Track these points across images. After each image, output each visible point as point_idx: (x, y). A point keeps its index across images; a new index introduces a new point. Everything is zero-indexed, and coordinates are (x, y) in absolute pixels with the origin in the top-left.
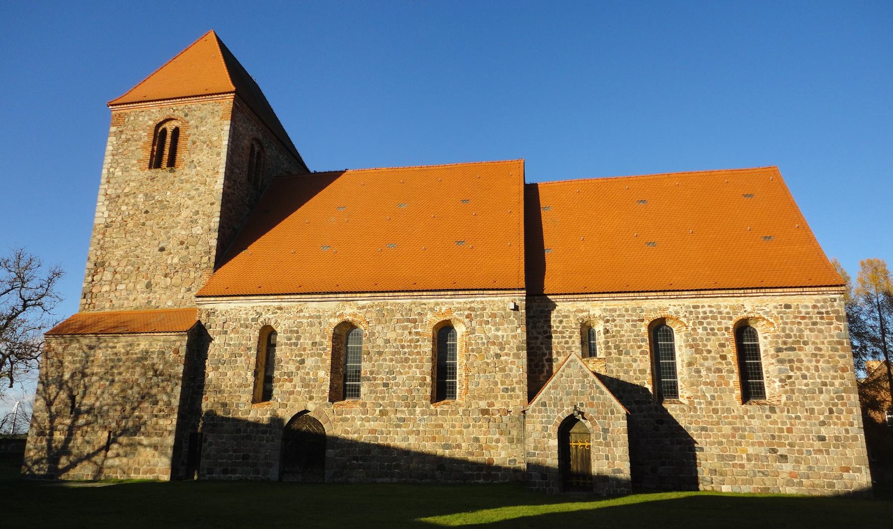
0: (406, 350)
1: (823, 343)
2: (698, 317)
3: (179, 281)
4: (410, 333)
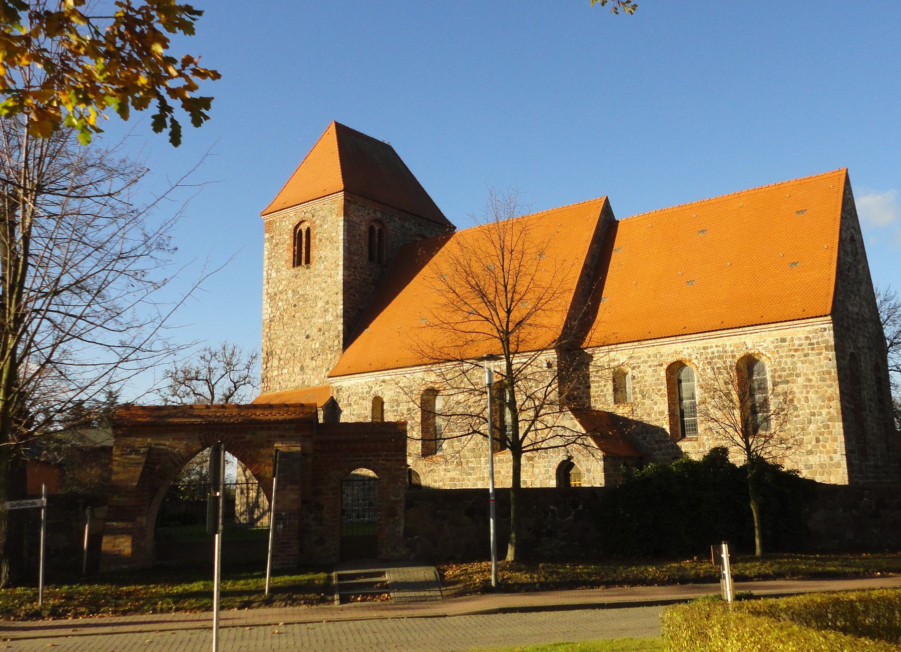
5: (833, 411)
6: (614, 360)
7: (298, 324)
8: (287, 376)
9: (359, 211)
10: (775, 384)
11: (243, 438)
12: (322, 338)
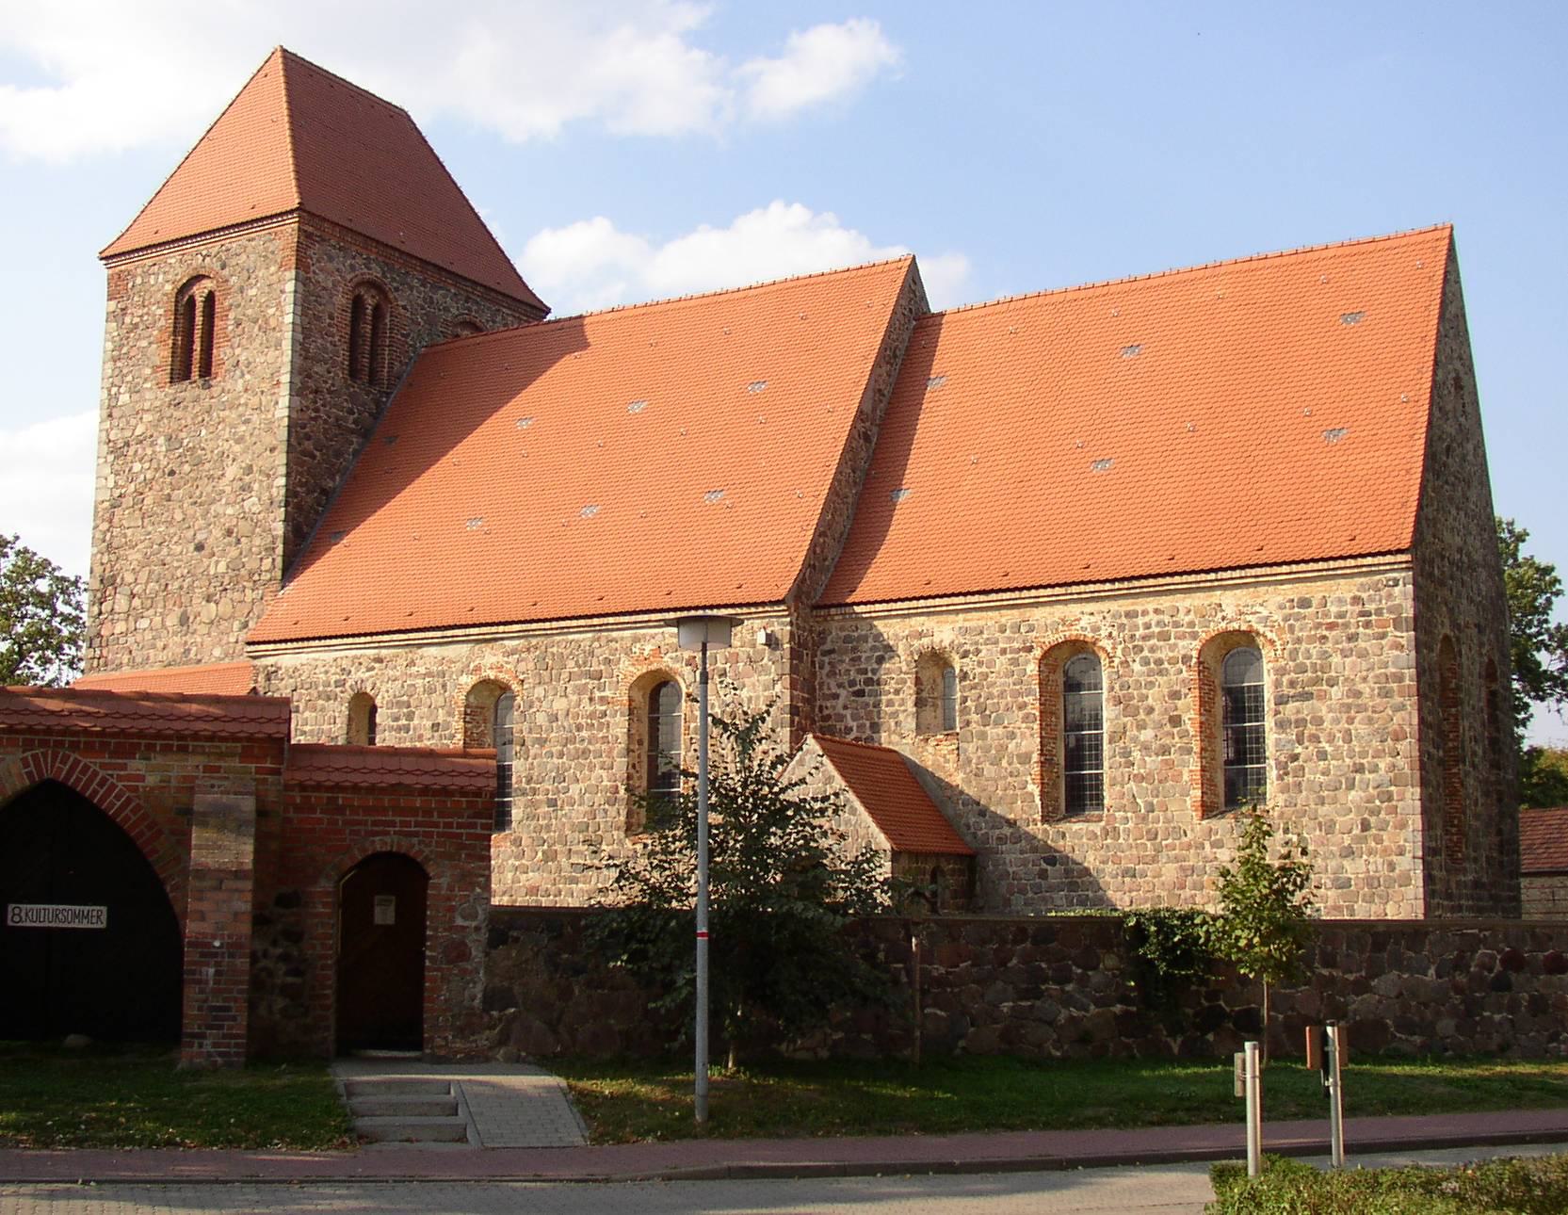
0: (584, 734)
1: (1365, 679)
2: (1133, 637)
3: (229, 609)
4: (591, 699)
5: (1400, 761)
6: (920, 635)
7: (179, 516)
8: (148, 636)
9: (331, 259)
10: (1281, 700)
11: (124, 767)
12: (234, 552)
